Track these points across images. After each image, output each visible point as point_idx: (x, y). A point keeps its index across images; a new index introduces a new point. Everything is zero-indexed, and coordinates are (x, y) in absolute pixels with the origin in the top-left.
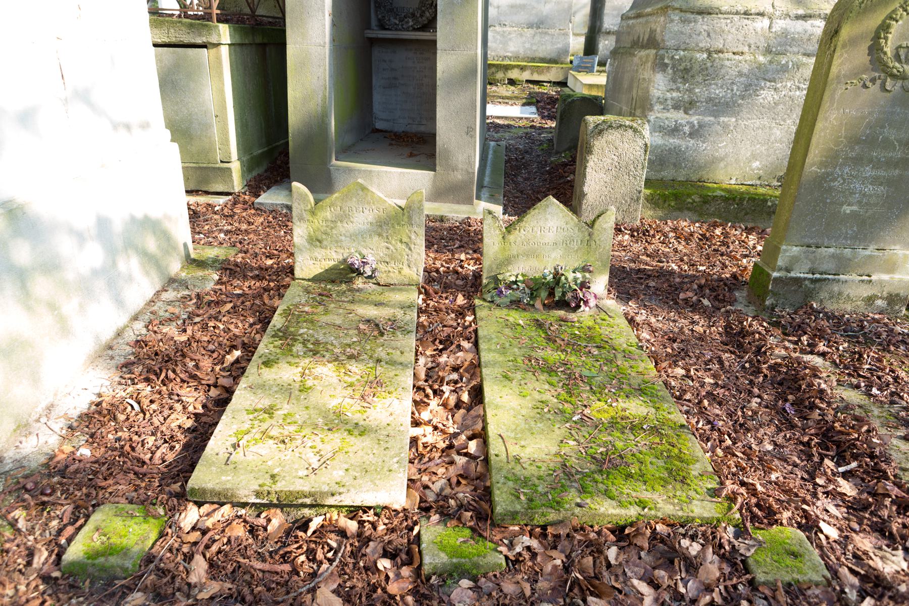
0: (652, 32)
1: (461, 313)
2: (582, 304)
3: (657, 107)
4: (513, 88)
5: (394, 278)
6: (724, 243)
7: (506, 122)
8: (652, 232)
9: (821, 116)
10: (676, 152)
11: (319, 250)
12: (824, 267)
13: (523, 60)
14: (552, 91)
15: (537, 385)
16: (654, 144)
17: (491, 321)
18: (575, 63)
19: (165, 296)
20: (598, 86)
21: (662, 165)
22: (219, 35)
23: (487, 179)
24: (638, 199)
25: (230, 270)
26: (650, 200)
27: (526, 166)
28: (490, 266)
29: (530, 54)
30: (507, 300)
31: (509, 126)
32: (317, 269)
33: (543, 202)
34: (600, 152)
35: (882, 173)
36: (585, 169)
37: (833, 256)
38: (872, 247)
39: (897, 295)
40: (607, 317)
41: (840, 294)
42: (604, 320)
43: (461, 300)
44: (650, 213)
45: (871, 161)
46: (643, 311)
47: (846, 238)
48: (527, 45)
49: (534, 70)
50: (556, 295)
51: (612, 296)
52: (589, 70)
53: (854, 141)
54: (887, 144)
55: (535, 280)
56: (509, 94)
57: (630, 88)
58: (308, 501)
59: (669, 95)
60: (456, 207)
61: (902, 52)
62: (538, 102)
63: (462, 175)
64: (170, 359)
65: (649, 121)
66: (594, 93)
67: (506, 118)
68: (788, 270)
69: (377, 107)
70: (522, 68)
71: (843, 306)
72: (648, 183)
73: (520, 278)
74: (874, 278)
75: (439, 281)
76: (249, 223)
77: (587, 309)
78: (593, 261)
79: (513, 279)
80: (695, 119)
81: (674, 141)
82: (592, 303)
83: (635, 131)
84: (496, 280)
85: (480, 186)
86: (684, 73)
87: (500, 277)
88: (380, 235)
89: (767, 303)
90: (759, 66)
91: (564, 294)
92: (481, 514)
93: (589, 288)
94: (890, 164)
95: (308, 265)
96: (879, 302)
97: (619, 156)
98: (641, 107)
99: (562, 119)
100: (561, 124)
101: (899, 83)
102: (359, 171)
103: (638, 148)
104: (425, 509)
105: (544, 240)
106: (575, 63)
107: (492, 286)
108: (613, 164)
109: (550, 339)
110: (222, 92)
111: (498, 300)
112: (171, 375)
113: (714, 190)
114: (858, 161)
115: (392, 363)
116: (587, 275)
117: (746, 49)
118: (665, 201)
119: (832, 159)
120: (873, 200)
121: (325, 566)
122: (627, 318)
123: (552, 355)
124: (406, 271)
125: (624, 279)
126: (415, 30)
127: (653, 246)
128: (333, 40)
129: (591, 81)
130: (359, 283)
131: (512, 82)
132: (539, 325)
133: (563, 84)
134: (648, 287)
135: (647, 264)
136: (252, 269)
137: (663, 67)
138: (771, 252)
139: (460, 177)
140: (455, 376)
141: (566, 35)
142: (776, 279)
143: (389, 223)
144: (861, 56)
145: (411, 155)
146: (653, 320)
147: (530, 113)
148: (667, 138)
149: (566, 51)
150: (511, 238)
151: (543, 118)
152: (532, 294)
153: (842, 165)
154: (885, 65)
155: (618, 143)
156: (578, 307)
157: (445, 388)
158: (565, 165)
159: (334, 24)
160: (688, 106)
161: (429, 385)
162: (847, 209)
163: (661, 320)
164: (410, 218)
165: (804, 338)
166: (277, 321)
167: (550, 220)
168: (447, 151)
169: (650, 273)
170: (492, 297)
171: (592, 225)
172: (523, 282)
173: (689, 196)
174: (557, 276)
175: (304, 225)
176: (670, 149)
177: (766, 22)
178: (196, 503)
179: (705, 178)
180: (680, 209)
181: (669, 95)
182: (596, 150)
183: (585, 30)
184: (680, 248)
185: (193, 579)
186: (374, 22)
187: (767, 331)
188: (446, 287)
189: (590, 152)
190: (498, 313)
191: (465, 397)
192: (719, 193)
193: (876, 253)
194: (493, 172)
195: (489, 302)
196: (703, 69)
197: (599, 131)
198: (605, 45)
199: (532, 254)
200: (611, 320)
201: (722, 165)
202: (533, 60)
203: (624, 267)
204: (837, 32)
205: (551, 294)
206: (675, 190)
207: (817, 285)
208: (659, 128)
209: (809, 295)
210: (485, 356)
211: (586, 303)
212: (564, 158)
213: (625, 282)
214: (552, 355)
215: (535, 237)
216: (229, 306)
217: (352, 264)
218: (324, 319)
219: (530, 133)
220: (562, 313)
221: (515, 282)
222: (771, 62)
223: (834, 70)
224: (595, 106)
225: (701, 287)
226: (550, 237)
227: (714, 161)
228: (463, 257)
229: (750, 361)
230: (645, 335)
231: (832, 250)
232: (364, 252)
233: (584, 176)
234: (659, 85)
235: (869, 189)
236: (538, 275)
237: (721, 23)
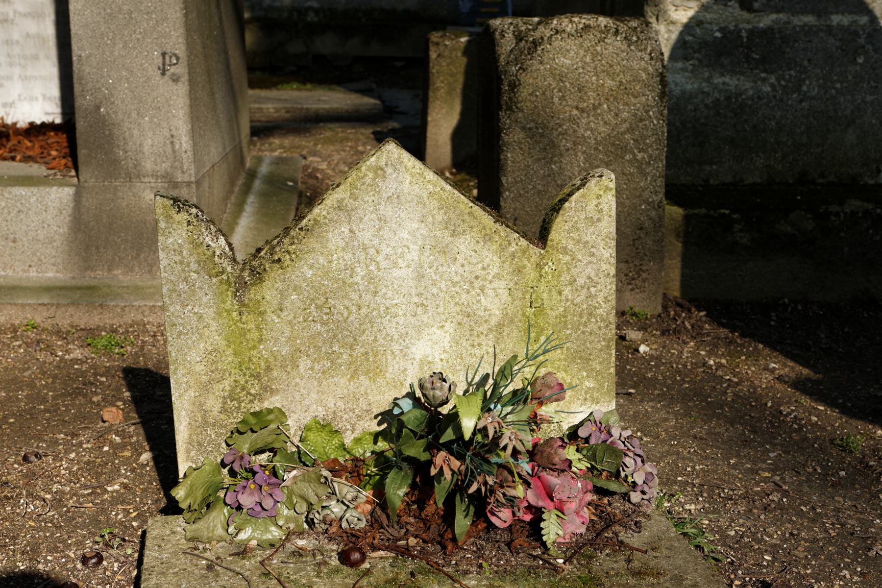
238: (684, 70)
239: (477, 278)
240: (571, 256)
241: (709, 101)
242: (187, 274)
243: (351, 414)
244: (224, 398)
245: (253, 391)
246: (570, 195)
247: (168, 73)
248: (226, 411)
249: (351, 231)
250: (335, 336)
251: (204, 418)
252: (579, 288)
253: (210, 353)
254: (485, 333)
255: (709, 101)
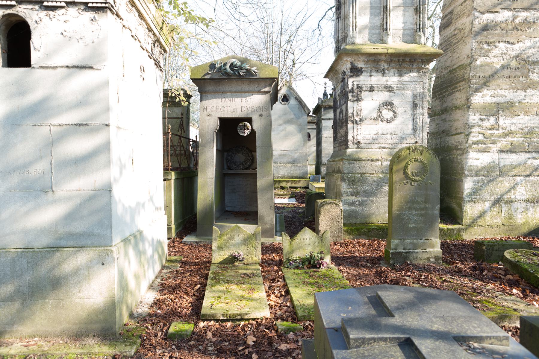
0: (339, 167)
1: (277, 272)
3: (344, 195)
4: (283, 191)
5: (250, 261)
6: (378, 247)
7: (283, 206)
9: (393, 195)
10: (354, 212)
11: (221, 252)
12: (409, 247)
13: (287, 178)
14: (302, 191)
15: (308, 288)
17: (288, 273)
18: (311, 178)
19: (163, 271)
20: (322, 188)
22: (171, 176)
23: (278, 229)
24: (341, 231)
25: (184, 264)
26: (347, 232)
27: (294, 223)
28: (286, 254)
29: (290, 175)
31: (284, 207)
32: (220, 259)
33: (304, 229)
35: (419, 212)
37: (410, 243)
38: (423, 239)
39: (438, 256)
41: (417, 257)
43: (276, 268)
44: (348, 237)
45: (414, 208)
47: (413, 236)
48: (288, 171)
49: (292, 182)
50: (311, 264)
52: (318, 181)
53: (407, 202)
54: (418, 203)
55: (303, 259)
56: (282, 193)
57: (334, 189)
58: (239, 317)
59: (348, 190)
60: (267, 239)
61: (414, 174)
62: (296, 196)
64: (175, 288)
65: (342, 201)
66: (321, 191)
67: (282, 204)
68: (396, 250)
69: (227, 201)
70: (287, 182)
71: (419, 262)
72: (345, 225)
73: (298, 258)
74: (427, 250)
75: (266, 262)
76: (182, 249)
79: (295, 259)
80: (360, 199)
81: (353, 208)
82: (325, 265)
83: (336, 204)
84: (288, 259)
85: (276, 231)
86: (352, 182)
87: (290, 258)
88: (245, 245)
89: (391, 262)
90: (381, 178)
91: (314, 262)
92: (295, 318)
94: (421, 209)
95: (218, 257)
96: (432, 260)
98: (338, 196)
99: (307, 202)
100: (307, 206)
101: (416, 183)
102: (226, 226)
104: (277, 319)
105: (306, 243)
106: (311, 178)
108: (330, 216)
109: (310, 276)
110: (170, 197)
111: (290, 267)
112: (178, 292)
113: (372, 226)
114: (410, 209)
115: (255, 284)
117: (374, 172)
119: (401, 209)
120: (419, 222)
121: (248, 332)
123: (311, 280)
124: (254, 258)
126: (243, 169)
128: (216, 176)
129: (319, 186)
130: (237, 264)
131: (283, 188)
132: (306, 273)
133: (307, 188)
136: (192, 263)
137: (344, 180)
138: (389, 243)
140: (278, 288)
141: (306, 166)
142: (392, 253)
143: (248, 240)
144: (401, 175)
145: (246, 220)
147: (293, 201)
149: (306, 173)
150: (293, 243)
151: (299, 203)
153: (405, 210)
154: (410, 178)
155: (330, 209)
157: (275, 291)
158: (311, 222)
159: (216, 170)
160: (356, 194)
161: (270, 290)
162: (411, 226)
163: (353, 271)
164: (256, 238)
165: (403, 272)
166: (211, 275)
167: (306, 236)
168: (262, 217)
171: (322, 237)
173: (362, 229)
174: (311, 256)
175: (216, 242)
177: (380, 163)
178: (202, 320)
179: (368, 221)
180: (360, 235)
181: (348, 190)
182: (322, 212)
183: (315, 163)
184: (360, 249)
185: (208, 338)
186: (226, 167)
187: (390, 271)
188: (269, 265)
189: (320, 214)
190: (291, 270)
191: (283, 293)
192: (374, 227)
193: (426, 241)
194: (280, 226)
196: (360, 180)
197: (322, 205)
198: (324, 170)
199: (301, 248)
201: (374, 216)
202: (292, 177)
204: (392, 168)
205: (310, 263)
206: (357, 226)
207: (408, 254)
208: (346, 203)
209: (405, 259)
210: (288, 281)
211: (323, 265)
212: (310, 219)
213: (337, 260)
214: (311, 280)
216: (189, 274)
217: (235, 256)
218: (227, 274)
219: (294, 210)
222: (384, 176)
223: (394, 180)
224: (321, 196)
225: (367, 260)
226: (307, 241)
227: (370, 215)
228: (274, 255)
229: (383, 280)
230: (345, 274)
231: (409, 241)
232: (239, 251)
233: (319, 223)
234: (344, 187)
235: (417, 218)
236: (304, 257)
237: (364, 164)
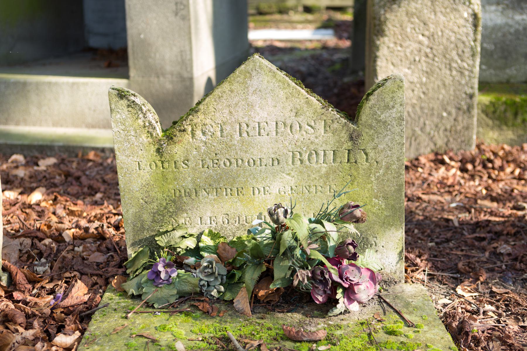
2: (339, 294)
8: (498, 163)
16: (490, 24)
21: (506, 58)
24: (470, 108)
28: (138, 217)
30: (169, 293)
34: (397, 31)
36: (375, 61)
40: (401, 327)
42: (391, 333)
43: (80, 292)
46: (488, 307)
51: (419, 275)
63: (172, 82)
72: (485, 86)
77: (354, 307)
78: (367, 196)
79: (191, 243)
82: (365, 290)
84: (153, 248)
87: (162, 241)
93: (354, 257)
97: (431, 37)
103: (461, 22)
107: (144, 260)
111: (151, 293)
116: (351, 228)
118: (516, 114)
122: (448, 327)
125: (448, 241)
127: (501, 185)
134: (496, 254)
135: (492, 213)
139: (169, 86)
145: (109, 66)
146: (513, 327)
147: (328, 37)
148: (510, 13)
150: (177, 150)
152: (231, 276)
155: (427, 13)
156: (332, 302)
169: (498, 228)
170: (139, 286)
172: (215, 250)
176: (517, 31)
189: (381, 33)
195: (133, 297)
199: (224, 180)
200: (410, 332)
203: (447, 220)
211: (350, 293)
215: (229, 147)
220: (293, 319)
221: (196, 252)
238: (496, 11)
239: (312, 143)
240: (374, 130)
241: (512, 30)
242: (129, 138)
243: (232, 226)
244: (154, 213)
245: (171, 210)
246: (374, 91)
247: (179, 14)
248: (155, 221)
249: (231, 112)
250: (221, 178)
251: (142, 225)
252: (380, 151)
253: (145, 186)
254: (317, 178)
255: (512, 30)
